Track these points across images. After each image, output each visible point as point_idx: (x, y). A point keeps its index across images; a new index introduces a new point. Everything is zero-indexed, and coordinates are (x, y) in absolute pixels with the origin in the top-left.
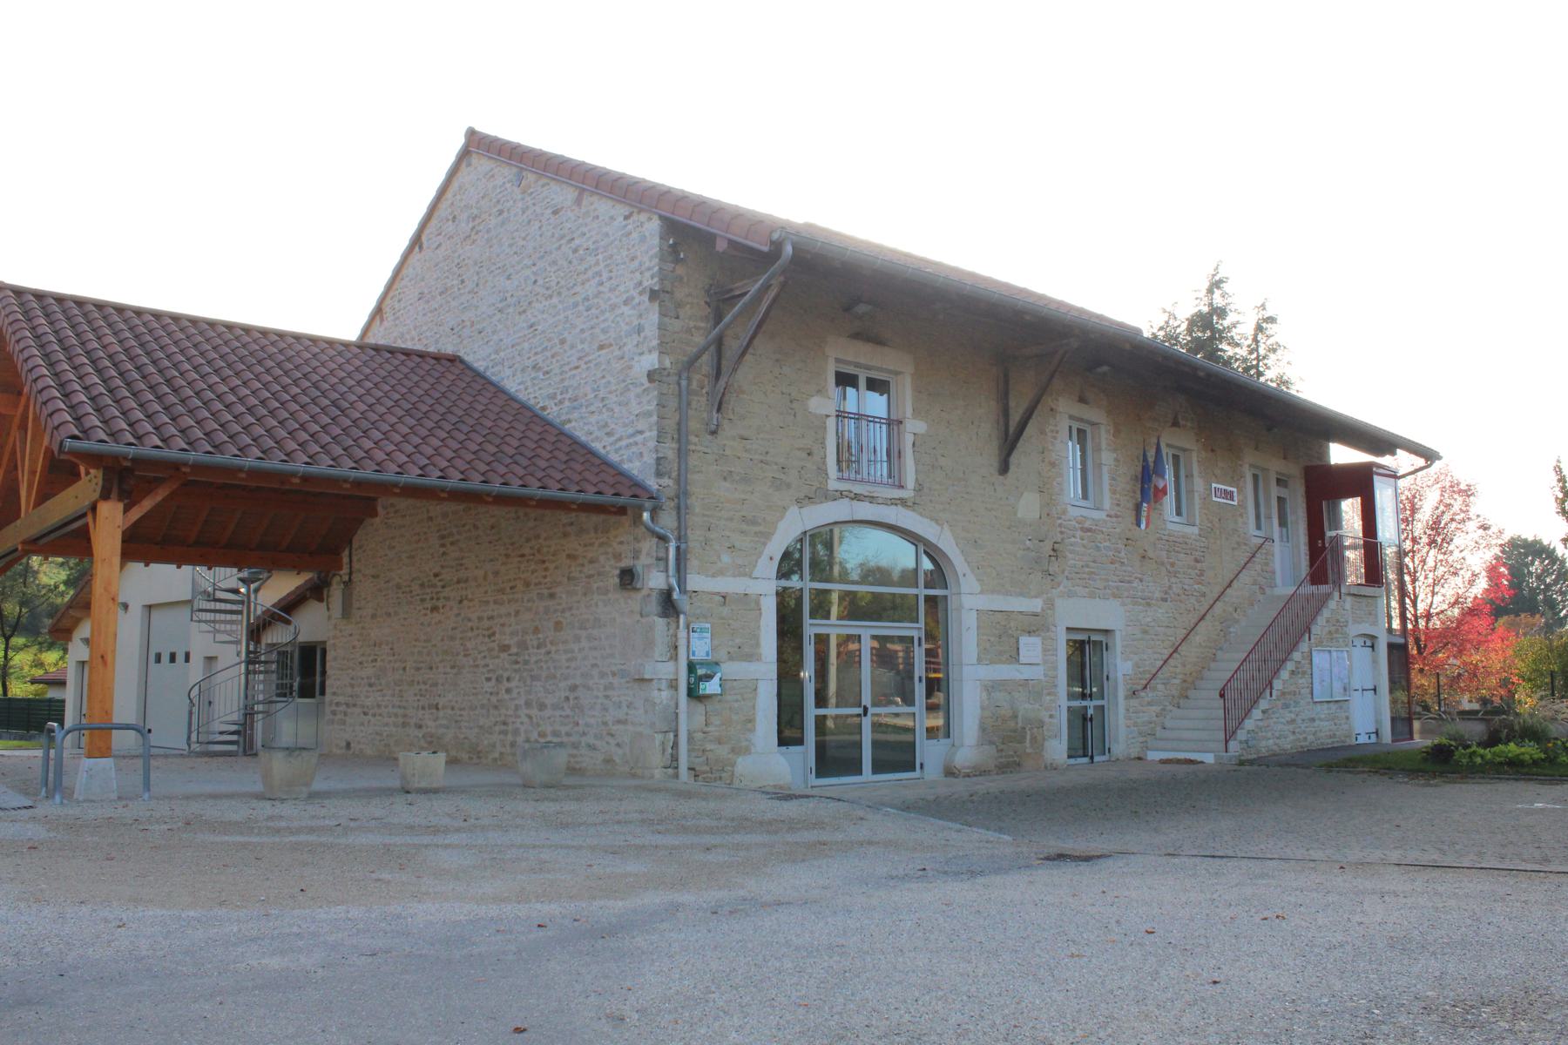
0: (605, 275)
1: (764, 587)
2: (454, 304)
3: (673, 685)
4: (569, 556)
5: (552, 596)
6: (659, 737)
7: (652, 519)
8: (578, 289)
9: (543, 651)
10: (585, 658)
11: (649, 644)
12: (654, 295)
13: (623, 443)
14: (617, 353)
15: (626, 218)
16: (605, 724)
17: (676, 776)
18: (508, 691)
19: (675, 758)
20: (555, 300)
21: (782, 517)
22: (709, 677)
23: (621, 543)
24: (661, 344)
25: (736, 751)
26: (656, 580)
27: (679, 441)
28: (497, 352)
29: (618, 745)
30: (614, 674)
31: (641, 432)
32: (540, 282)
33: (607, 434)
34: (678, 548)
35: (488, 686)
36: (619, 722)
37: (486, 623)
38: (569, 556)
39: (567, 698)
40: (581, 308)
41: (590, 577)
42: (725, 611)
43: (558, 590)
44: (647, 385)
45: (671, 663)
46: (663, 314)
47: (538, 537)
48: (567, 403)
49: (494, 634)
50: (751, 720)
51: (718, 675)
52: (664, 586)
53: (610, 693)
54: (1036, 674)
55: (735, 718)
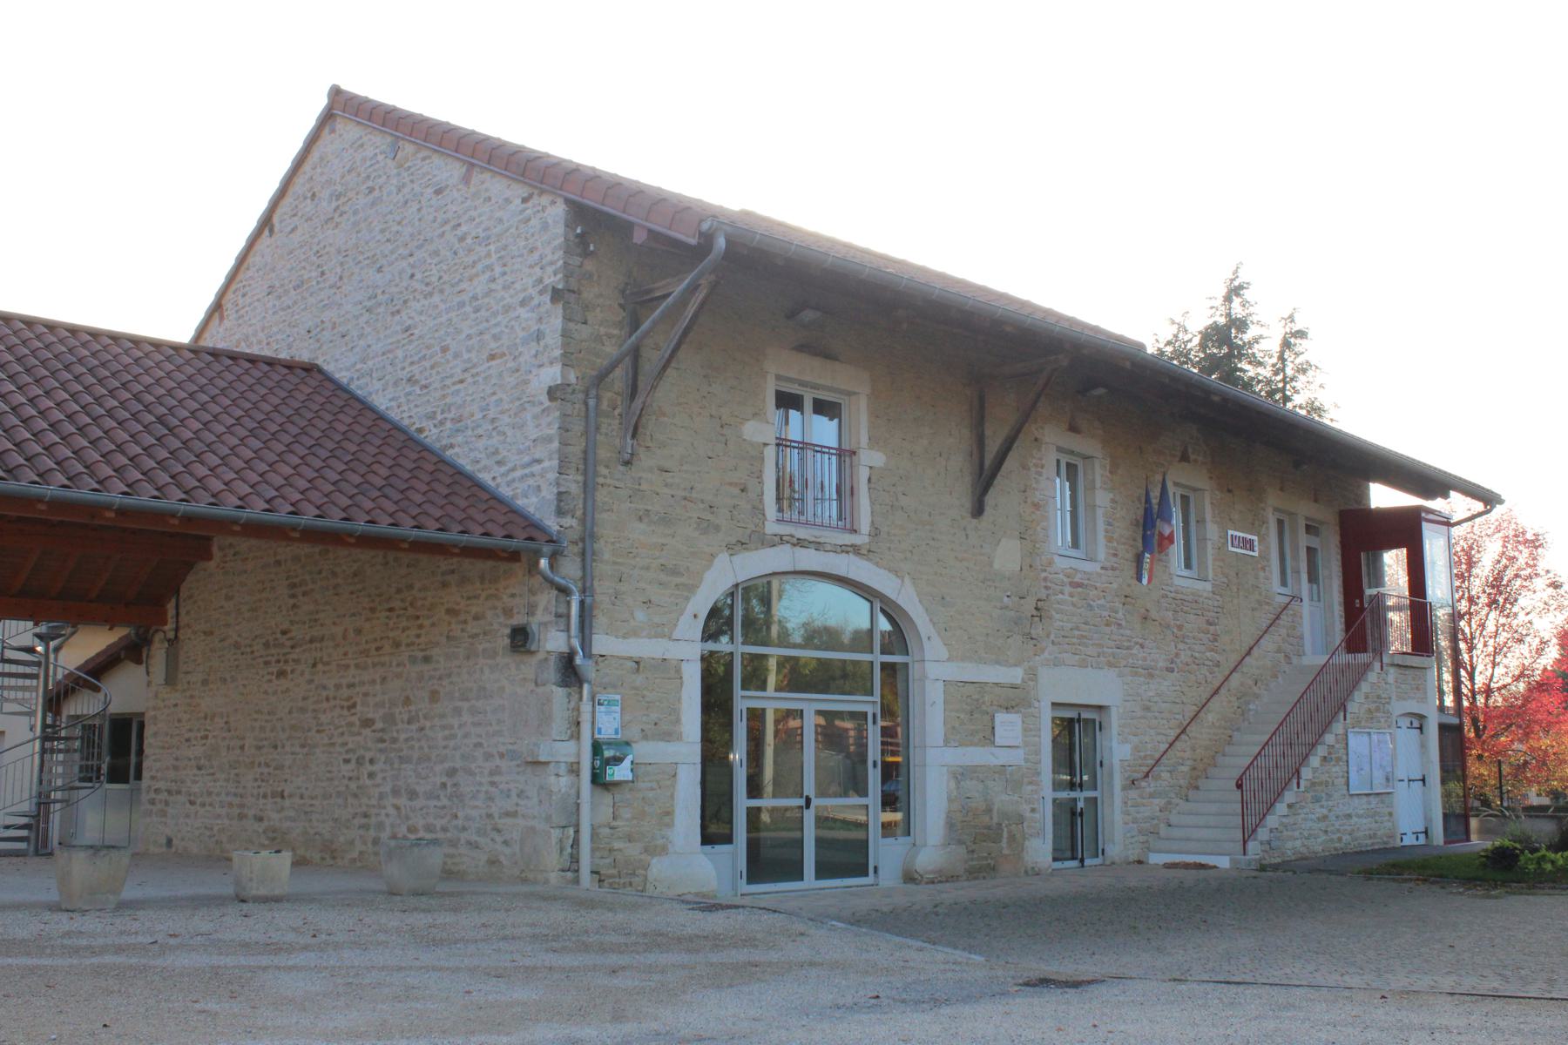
0: (498, 270)
1: (686, 650)
3: (574, 770)
5: (427, 659)
6: (555, 834)
8: (463, 286)
9: (414, 727)
10: (466, 736)
13: (518, 474)
14: (511, 364)
16: (490, 816)
17: (577, 881)
18: (371, 775)
19: (575, 859)
20: (436, 298)
21: (709, 567)
22: (618, 760)
23: (513, 595)
24: (565, 355)
26: (554, 641)
27: (585, 473)
28: (364, 361)
31: (539, 461)
32: (418, 276)
34: (582, 603)
36: (508, 814)
37: (345, 692)
40: (468, 309)
42: (639, 680)
43: (435, 652)
45: (572, 743)
46: (567, 318)
48: (449, 425)
51: (630, 757)
52: (565, 649)
53: (496, 779)
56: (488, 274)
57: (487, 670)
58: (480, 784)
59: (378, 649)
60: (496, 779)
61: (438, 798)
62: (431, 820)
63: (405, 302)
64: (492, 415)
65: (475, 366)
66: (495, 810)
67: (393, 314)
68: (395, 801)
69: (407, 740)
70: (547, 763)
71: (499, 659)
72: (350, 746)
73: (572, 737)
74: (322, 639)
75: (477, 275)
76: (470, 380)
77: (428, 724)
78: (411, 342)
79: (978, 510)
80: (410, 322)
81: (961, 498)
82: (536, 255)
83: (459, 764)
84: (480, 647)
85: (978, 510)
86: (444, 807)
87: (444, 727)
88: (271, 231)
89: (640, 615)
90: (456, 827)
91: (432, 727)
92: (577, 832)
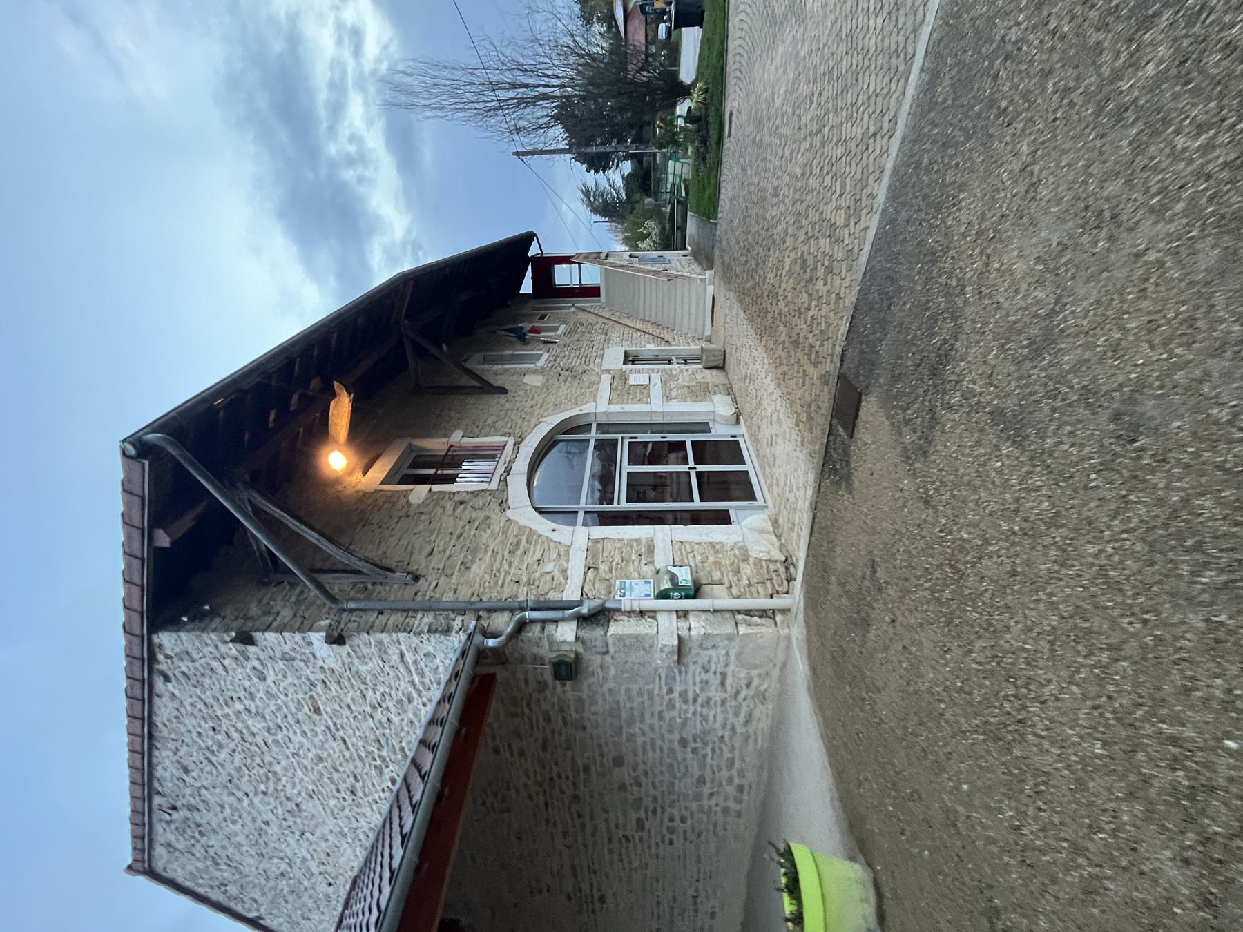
0: (239, 706)
1: (580, 536)
2: (305, 883)
3: (683, 614)
4: (544, 749)
5: (586, 769)
6: (743, 630)
7: (494, 636)
8: (259, 740)
9: (643, 780)
10: (652, 728)
11: (638, 642)
12: (245, 639)
13: (416, 679)
14: (319, 687)
15: (167, 679)
16: (723, 702)
17: (784, 611)
18: (683, 820)
19: (763, 613)
20: (278, 768)
21: (516, 523)
22: (673, 578)
23: (526, 681)
24: (300, 630)
25: (745, 558)
26: (566, 632)
27: (416, 611)
28: (345, 836)
29: (748, 685)
30: (670, 691)
31: (402, 656)
32: (262, 787)
33: (410, 702)
34: (533, 609)
35: (678, 841)
36: (723, 683)
37: (616, 845)
38: (544, 749)
39: (694, 751)
40: (279, 736)
41: (565, 721)
42: (603, 567)
43: (580, 762)
44: (347, 648)
45: (659, 616)
46: (267, 628)
47: (526, 786)
48: (384, 753)
49: (626, 837)
50: (712, 545)
51: (670, 568)
52: (574, 625)
53: (691, 695)
54: (656, 378)
55: (711, 559)
56: (245, 716)
57: (594, 708)
58: (694, 713)
59: (580, 816)
60: (691, 695)
61: (705, 756)
62: (723, 764)
63: (288, 799)
64: (368, 709)
65: (328, 728)
66: (717, 697)
67: (300, 811)
68: (705, 798)
69: (654, 788)
70: (679, 637)
71: (585, 696)
72: (659, 839)
73: (654, 618)
74: (573, 867)
75: (248, 728)
76: (341, 733)
77: (642, 767)
78: (320, 793)
79: (503, 391)
80: (303, 794)
81: (502, 399)
82: (215, 664)
83: (676, 736)
84: (574, 715)
85: (503, 391)
86: (713, 750)
87: (644, 750)
88: (260, 918)
89: (549, 567)
90: (731, 737)
91: (645, 763)
92: (739, 612)
